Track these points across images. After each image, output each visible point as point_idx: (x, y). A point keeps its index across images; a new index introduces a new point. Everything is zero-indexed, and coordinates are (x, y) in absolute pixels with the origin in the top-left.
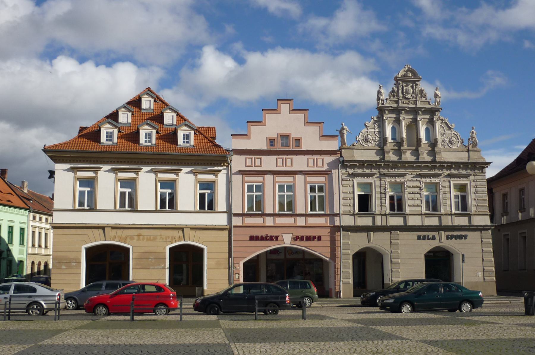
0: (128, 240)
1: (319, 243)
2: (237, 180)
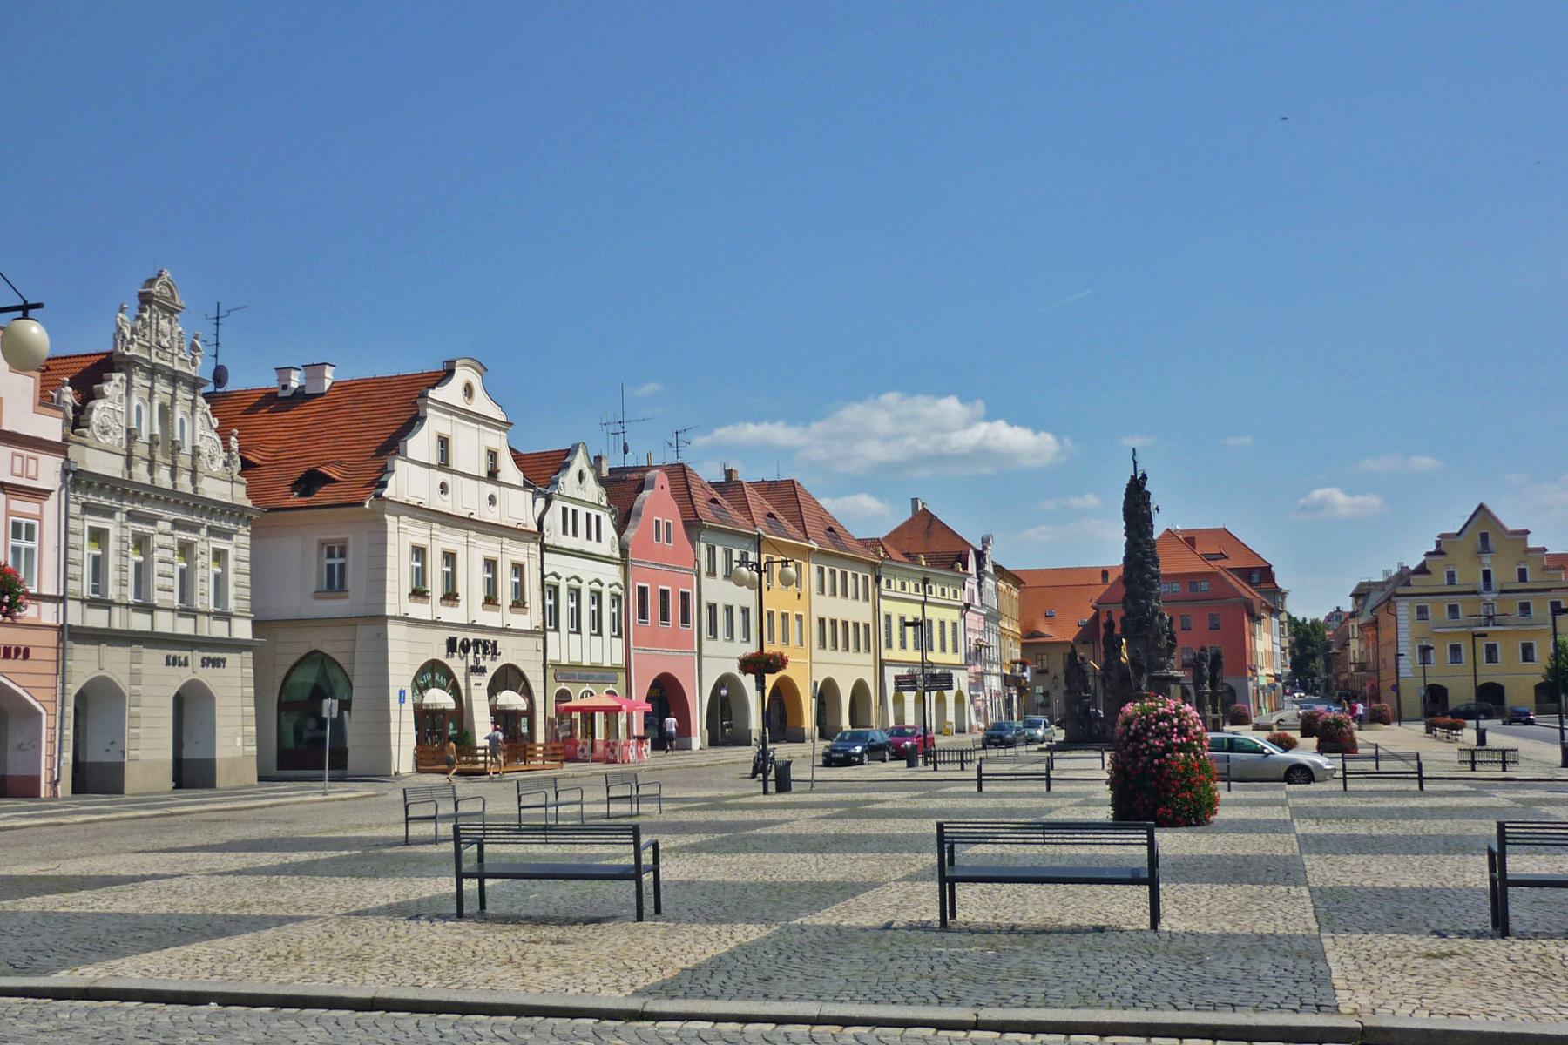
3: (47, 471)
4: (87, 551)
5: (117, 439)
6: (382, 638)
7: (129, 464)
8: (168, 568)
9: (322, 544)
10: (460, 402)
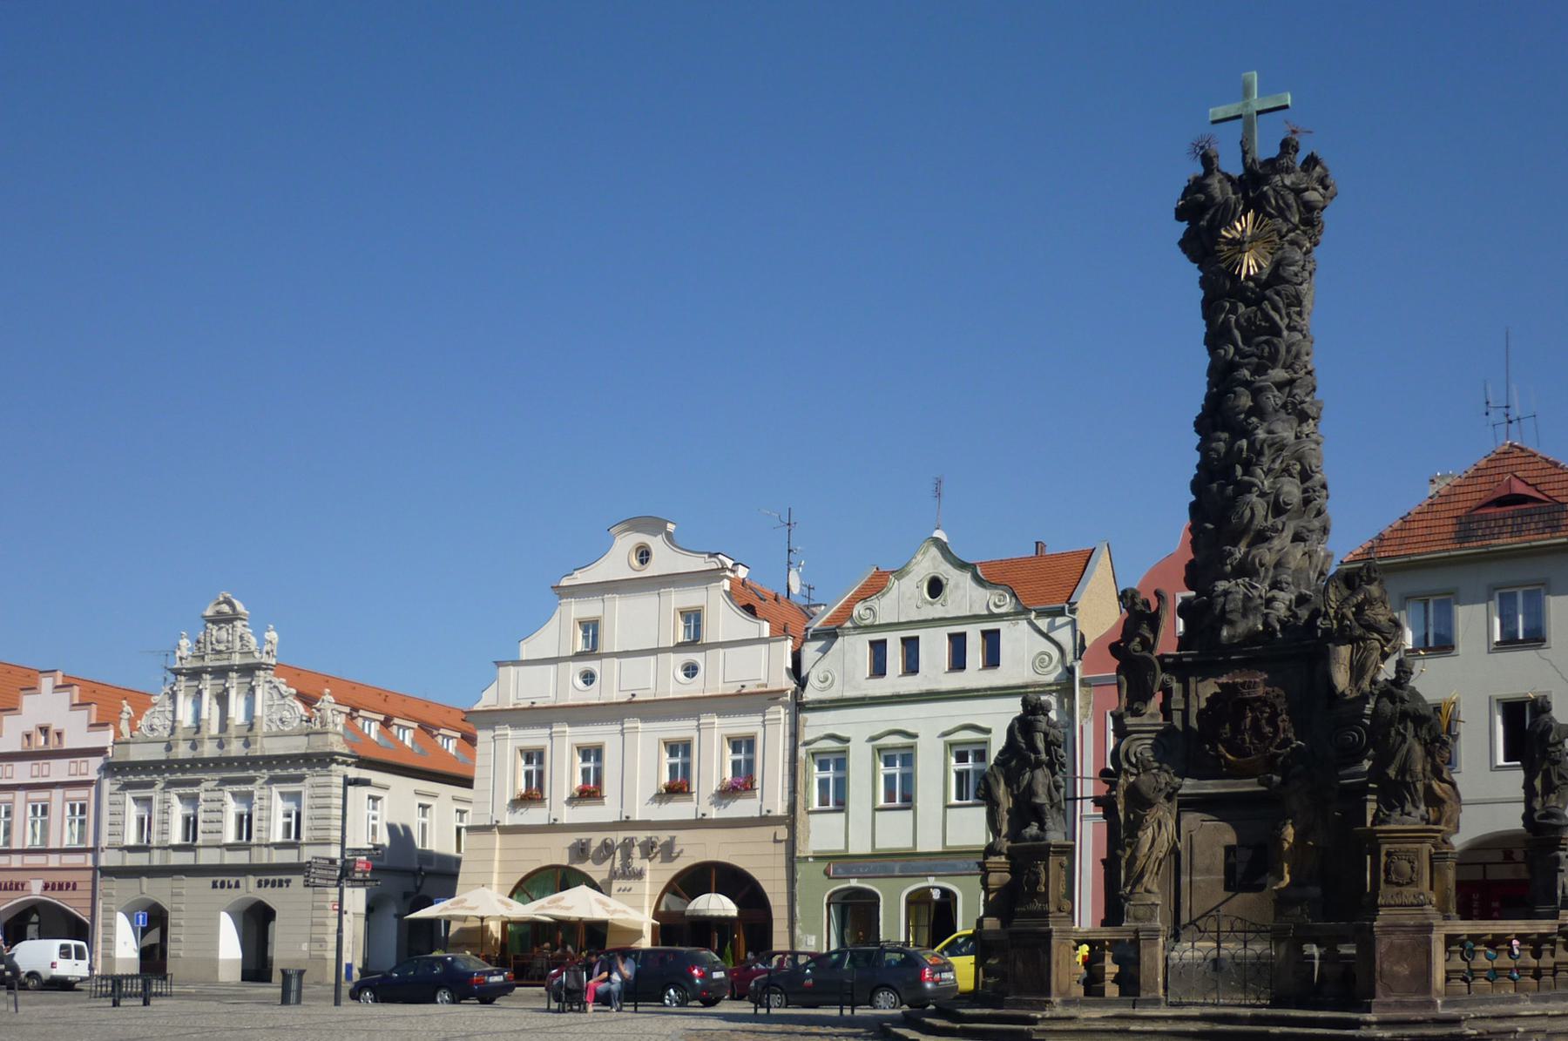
3: (91, 768)
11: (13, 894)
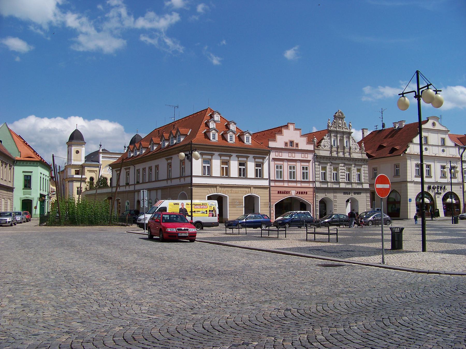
0: (227, 192)
1: (307, 195)
2: (272, 163)
3: (310, 157)
4: (321, 171)
5: (328, 148)
6: (406, 186)
7: (331, 153)
8: (343, 174)
9: (395, 165)
10: (431, 127)
11: (284, 195)
